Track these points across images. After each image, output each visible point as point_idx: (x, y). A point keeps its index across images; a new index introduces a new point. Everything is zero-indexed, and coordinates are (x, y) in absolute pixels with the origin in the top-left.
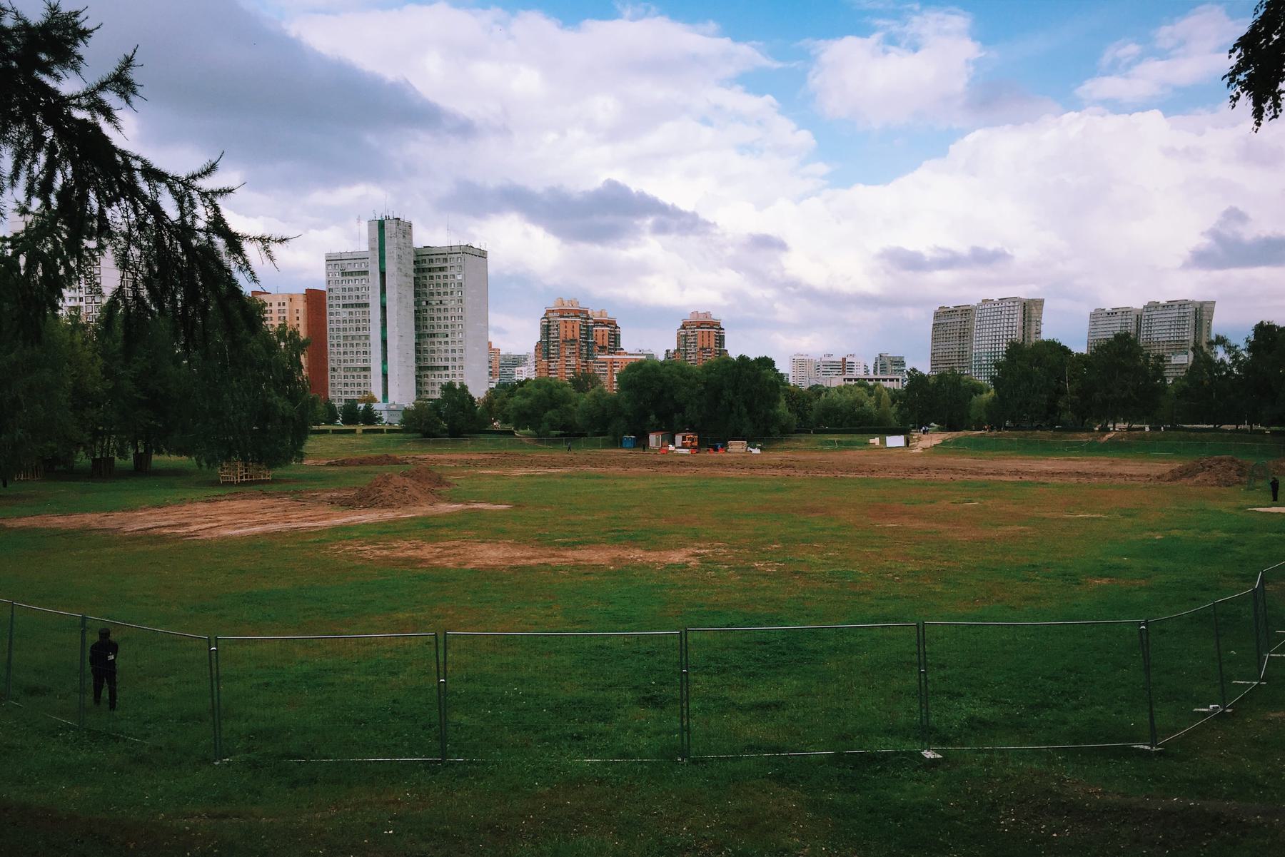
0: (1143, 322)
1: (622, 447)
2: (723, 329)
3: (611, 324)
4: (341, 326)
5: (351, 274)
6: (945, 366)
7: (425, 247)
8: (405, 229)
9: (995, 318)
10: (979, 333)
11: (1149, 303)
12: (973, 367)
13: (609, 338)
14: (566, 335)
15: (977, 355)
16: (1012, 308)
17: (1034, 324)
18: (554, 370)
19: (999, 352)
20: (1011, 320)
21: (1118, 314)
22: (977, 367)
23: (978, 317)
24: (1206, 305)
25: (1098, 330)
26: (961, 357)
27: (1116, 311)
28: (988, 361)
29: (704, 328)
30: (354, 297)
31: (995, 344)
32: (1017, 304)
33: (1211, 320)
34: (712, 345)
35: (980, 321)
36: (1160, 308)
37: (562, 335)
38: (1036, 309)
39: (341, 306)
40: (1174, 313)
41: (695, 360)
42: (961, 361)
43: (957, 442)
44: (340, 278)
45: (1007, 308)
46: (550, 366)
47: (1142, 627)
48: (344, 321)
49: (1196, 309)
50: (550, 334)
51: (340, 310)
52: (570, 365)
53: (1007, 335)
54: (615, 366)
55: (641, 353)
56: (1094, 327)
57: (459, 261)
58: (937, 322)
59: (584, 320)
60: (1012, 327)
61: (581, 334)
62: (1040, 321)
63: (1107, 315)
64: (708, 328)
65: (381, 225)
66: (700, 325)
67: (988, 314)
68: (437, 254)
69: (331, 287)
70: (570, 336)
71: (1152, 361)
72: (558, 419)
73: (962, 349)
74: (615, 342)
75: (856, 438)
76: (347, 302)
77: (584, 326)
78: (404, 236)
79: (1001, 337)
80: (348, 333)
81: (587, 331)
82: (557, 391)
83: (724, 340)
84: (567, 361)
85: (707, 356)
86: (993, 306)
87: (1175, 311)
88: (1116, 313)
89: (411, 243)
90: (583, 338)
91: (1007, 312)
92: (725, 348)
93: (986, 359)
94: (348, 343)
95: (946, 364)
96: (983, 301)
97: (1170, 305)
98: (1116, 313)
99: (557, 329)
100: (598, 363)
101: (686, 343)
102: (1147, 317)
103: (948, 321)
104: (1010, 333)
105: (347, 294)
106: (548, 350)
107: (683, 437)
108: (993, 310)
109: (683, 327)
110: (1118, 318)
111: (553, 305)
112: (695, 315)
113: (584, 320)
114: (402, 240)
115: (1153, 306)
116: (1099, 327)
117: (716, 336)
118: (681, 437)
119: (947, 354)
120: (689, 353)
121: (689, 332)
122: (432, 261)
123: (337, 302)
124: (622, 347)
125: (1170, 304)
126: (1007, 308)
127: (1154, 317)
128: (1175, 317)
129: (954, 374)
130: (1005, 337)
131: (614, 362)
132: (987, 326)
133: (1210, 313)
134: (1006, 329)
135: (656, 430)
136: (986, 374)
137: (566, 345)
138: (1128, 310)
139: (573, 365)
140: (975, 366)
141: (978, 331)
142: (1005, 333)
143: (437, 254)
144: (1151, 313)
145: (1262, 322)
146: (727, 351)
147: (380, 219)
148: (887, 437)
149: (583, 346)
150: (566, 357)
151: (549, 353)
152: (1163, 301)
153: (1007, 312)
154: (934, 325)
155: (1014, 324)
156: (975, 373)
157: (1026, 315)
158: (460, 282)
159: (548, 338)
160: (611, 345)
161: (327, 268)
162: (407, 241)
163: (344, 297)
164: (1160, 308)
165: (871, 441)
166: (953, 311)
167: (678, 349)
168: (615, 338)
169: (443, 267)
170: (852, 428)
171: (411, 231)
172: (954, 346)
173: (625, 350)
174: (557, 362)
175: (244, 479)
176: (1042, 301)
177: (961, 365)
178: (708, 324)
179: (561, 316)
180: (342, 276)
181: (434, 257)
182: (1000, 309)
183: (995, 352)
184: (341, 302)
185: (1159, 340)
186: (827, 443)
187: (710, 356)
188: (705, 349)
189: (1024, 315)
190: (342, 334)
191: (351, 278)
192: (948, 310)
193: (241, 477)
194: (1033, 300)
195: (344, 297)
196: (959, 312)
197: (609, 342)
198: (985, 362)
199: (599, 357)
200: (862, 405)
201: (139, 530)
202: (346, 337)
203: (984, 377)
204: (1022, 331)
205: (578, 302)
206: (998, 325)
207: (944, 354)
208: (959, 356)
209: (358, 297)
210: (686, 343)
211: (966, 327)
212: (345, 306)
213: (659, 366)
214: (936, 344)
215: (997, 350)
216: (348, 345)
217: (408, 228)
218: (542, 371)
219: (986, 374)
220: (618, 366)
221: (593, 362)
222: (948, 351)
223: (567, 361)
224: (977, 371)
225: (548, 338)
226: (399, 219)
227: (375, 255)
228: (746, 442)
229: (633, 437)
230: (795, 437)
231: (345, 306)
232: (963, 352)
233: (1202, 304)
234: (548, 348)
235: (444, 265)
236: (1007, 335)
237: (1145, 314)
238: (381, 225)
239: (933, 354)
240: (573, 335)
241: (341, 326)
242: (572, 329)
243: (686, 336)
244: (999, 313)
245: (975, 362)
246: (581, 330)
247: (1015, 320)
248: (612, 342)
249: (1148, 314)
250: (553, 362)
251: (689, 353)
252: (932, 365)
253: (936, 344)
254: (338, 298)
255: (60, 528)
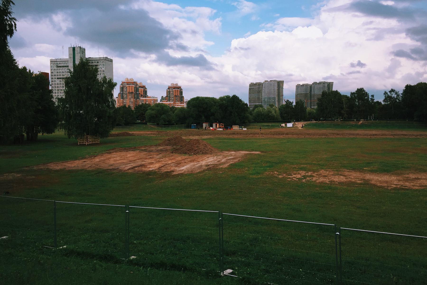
0: (312, 89)
1: (191, 128)
2: (182, 89)
3: (144, 87)
4: (56, 86)
5: (60, 67)
6: (253, 102)
7: (89, 58)
8: (83, 51)
9: (269, 86)
10: (264, 91)
11: (314, 82)
13: (143, 92)
14: (129, 91)
15: (264, 98)
17: (281, 88)
18: (125, 103)
19: (271, 97)
20: (274, 87)
23: (264, 86)
24: (331, 83)
25: (299, 91)
26: (258, 99)
27: (304, 85)
29: (176, 89)
30: (61, 75)
31: (269, 95)
32: (276, 82)
33: (332, 88)
34: (179, 95)
37: (128, 90)
38: (282, 84)
39: (56, 78)
40: (321, 86)
41: (173, 100)
43: (309, 125)
44: (56, 68)
45: (273, 84)
46: (123, 101)
48: (58, 84)
49: (328, 84)
50: (123, 90)
51: (56, 80)
52: (131, 101)
53: (273, 92)
54: (147, 102)
55: (153, 97)
56: (297, 90)
57: (103, 63)
58: (250, 88)
59: (135, 86)
61: (135, 90)
62: (283, 88)
63: (301, 86)
64: (177, 89)
65: (74, 49)
66: (174, 88)
67: (267, 85)
68: (94, 60)
69: (52, 72)
70: (131, 91)
71: (370, 97)
72: (166, 118)
73: (258, 97)
74: (145, 93)
75: (277, 124)
76: (59, 77)
77: (136, 88)
78: (82, 53)
80: (59, 88)
81: (137, 89)
82: (165, 108)
83: (182, 93)
84: (130, 100)
85: (177, 98)
87: (322, 85)
88: (304, 86)
89: (85, 56)
90: (135, 92)
91: (273, 85)
92: (183, 96)
93: (267, 99)
94: (59, 92)
97: (320, 83)
98: (304, 86)
99: (126, 89)
100: (141, 100)
101: (170, 94)
102: (313, 87)
103: (254, 87)
104: (274, 91)
105: (59, 74)
106: (123, 96)
107: (216, 124)
108: (268, 84)
109: (169, 89)
110: (304, 87)
111: (126, 80)
112: (173, 85)
113: (135, 86)
114: (82, 55)
115: (315, 83)
117: (180, 92)
120: (171, 97)
121: (171, 90)
122: (93, 62)
123: (55, 77)
124: (148, 95)
125: (320, 83)
126: (273, 84)
127: (315, 87)
128: (322, 86)
130: (272, 93)
131: (147, 100)
132: (268, 88)
134: (272, 90)
136: (267, 104)
137: (130, 94)
138: (307, 84)
139: (132, 101)
141: (264, 91)
142: (272, 91)
143: (94, 60)
145: (407, 85)
146: (183, 96)
147: (73, 47)
148: (287, 124)
149: (135, 95)
150: (130, 98)
151: (123, 97)
152: (318, 82)
153: (273, 85)
156: (263, 104)
157: (279, 86)
158: (104, 70)
159: (123, 92)
160: (144, 95)
161: (51, 65)
162: (84, 55)
163: (58, 75)
165: (282, 125)
166: (255, 84)
167: (167, 96)
168: (145, 92)
169: (97, 65)
170: (284, 120)
171: (85, 52)
172: (256, 96)
173: (149, 96)
174: (126, 100)
175: (90, 143)
177: (258, 101)
178: (177, 88)
179: (128, 84)
180: (57, 67)
181: (93, 61)
182: (270, 84)
183: (269, 97)
184: (56, 77)
187: (178, 98)
188: (176, 96)
190: (56, 89)
191: (60, 68)
193: (89, 142)
195: (58, 75)
196: (257, 85)
197: (143, 93)
198: (266, 101)
199: (141, 98)
200: (271, 113)
201: (129, 169)
202: (58, 90)
203: (266, 105)
204: (278, 91)
205: (133, 80)
207: (253, 98)
208: (258, 99)
209: (63, 75)
210: (170, 94)
212: (58, 78)
216: (59, 93)
217: (84, 50)
218: (121, 103)
220: (148, 102)
221: (139, 100)
223: (130, 100)
225: (123, 92)
226: (80, 47)
227: (71, 60)
228: (238, 126)
229: (195, 124)
231: (58, 78)
232: (259, 97)
233: (330, 83)
234: (123, 95)
235: (97, 64)
236: (273, 92)
238: (74, 49)
239: (249, 98)
240: (132, 91)
241: (56, 86)
242: (132, 89)
243: (170, 91)
246: (134, 89)
248: (144, 93)
249: (314, 86)
250: (125, 100)
251: (171, 97)
252: (249, 101)
254: (55, 75)
255: (65, 168)
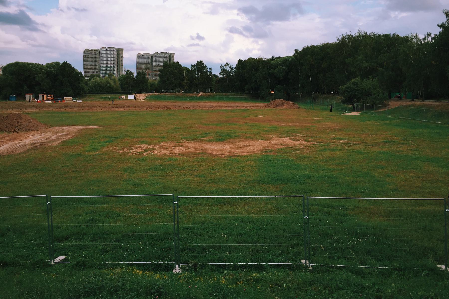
11: (155, 52)
12: (100, 71)
15: (101, 67)
16: (113, 51)
17: (120, 57)
19: (109, 66)
21: (146, 55)
22: (102, 73)
24: (172, 54)
27: (145, 54)
28: (105, 69)
31: (109, 64)
32: (114, 50)
33: (173, 59)
35: (102, 55)
36: (159, 54)
42: (95, 69)
43: (150, 97)
45: (111, 51)
47: (175, 202)
58: (85, 54)
60: (113, 58)
71: (209, 70)
79: (110, 61)
86: (106, 50)
87: (163, 56)
88: (145, 55)
91: (111, 52)
93: (104, 68)
95: (90, 70)
96: (102, 48)
97: (162, 54)
98: (145, 55)
115: (156, 54)
116: (140, 59)
118: (42, 95)
119: (90, 66)
129: (143, 72)
133: (85, 57)
134: (111, 58)
135: (28, 93)
136: (105, 74)
138: (148, 54)
140: (101, 71)
144: (156, 56)
152: (159, 52)
153: (111, 52)
154: (84, 55)
155: (114, 57)
156: (101, 74)
157: (118, 54)
164: (159, 54)
165: (122, 97)
166: (91, 51)
176: (123, 49)
177: (95, 70)
185: (159, 65)
186: (101, 98)
189: (117, 54)
192: (88, 50)
194: (120, 49)
196: (93, 51)
198: (104, 70)
206: (108, 57)
207: (88, 66)
211: (96, 57)
213: (27, 65)
214: (85, 62)
215: (108, 66)
219: (105, 74)
222: (90, 65)
224: (102, 73)
229: (15, 96)
230: (88, 95)
233: (171, 54)
237: (154, 56)
244: (108, 53)
245: (101, 69)
247: (114, 55)
253: (85, 62)
